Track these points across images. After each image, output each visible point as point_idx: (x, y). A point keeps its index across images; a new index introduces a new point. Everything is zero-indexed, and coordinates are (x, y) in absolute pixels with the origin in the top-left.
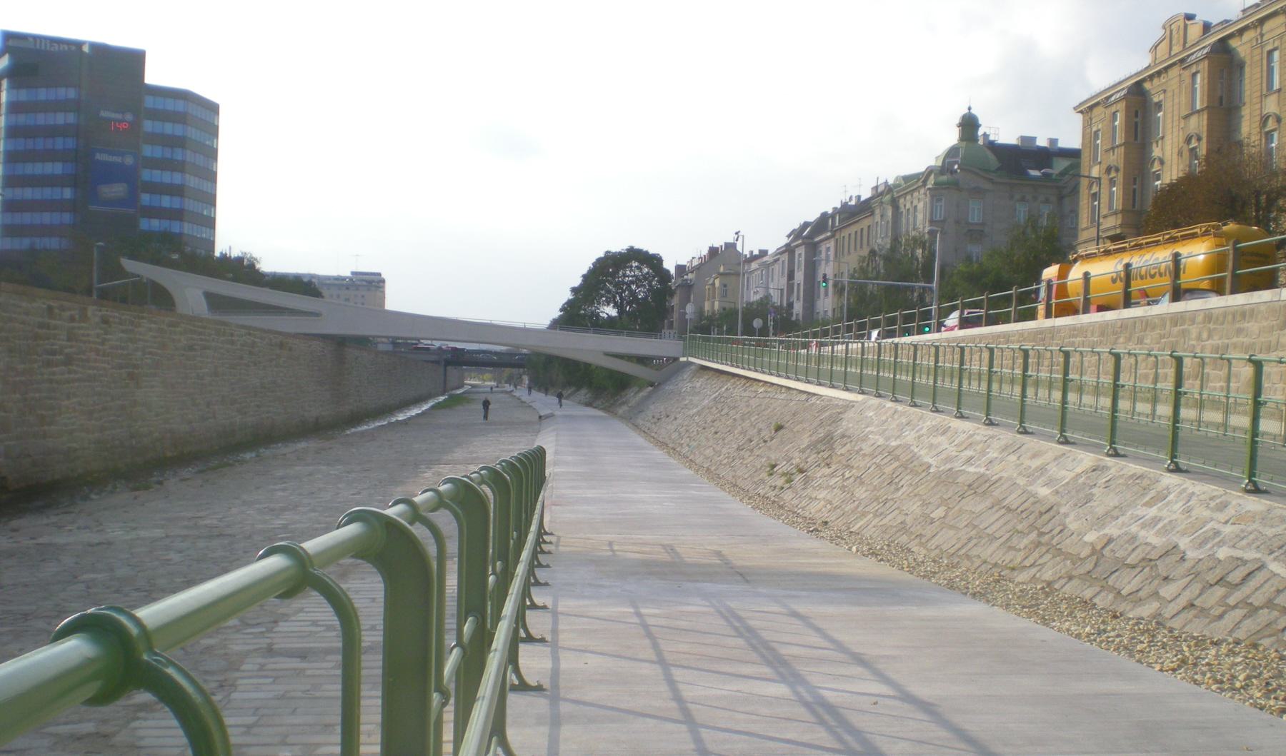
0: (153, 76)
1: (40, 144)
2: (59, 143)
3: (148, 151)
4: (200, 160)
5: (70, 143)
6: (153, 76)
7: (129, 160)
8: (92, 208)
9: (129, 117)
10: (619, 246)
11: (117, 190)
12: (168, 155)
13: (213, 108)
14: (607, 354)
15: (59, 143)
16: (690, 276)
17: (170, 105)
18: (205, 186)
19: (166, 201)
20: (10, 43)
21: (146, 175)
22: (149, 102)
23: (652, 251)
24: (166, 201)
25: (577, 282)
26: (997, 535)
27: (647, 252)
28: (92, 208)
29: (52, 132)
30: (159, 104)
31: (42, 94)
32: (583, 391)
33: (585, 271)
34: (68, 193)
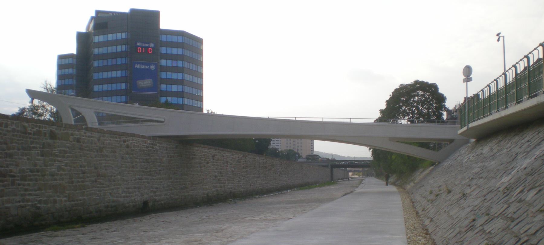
0: (165, 24)
1: (110, 62)
2: (119, 61)
3: (164, 62)
4: (192, 67)
5: (124, 61)
6: (165, 24)
7: (153, 67)
8: (134, 92)
9: (152, 45)
10: (409, 80)
11: (147, 83)
12: (175, 65)
13: (199, 41)
14: (392, 139)
15: (119, 61)
16: (455, 114)
17: (175, 39)
18: (197, 80)
19: (174, 88)
20: (99, 15)
21: (164, 75)
22: (164, 38)
23: (430, 82)
24: (174, 88)
25: (384, 107)
26: (515, 216)
27: (427, 83)
28: (134, 92)
29: (115, 55)
30: (169, 38)
31: (110, 37)
32: (394, 176)
33: (388, 98)
34: (123, 86)
